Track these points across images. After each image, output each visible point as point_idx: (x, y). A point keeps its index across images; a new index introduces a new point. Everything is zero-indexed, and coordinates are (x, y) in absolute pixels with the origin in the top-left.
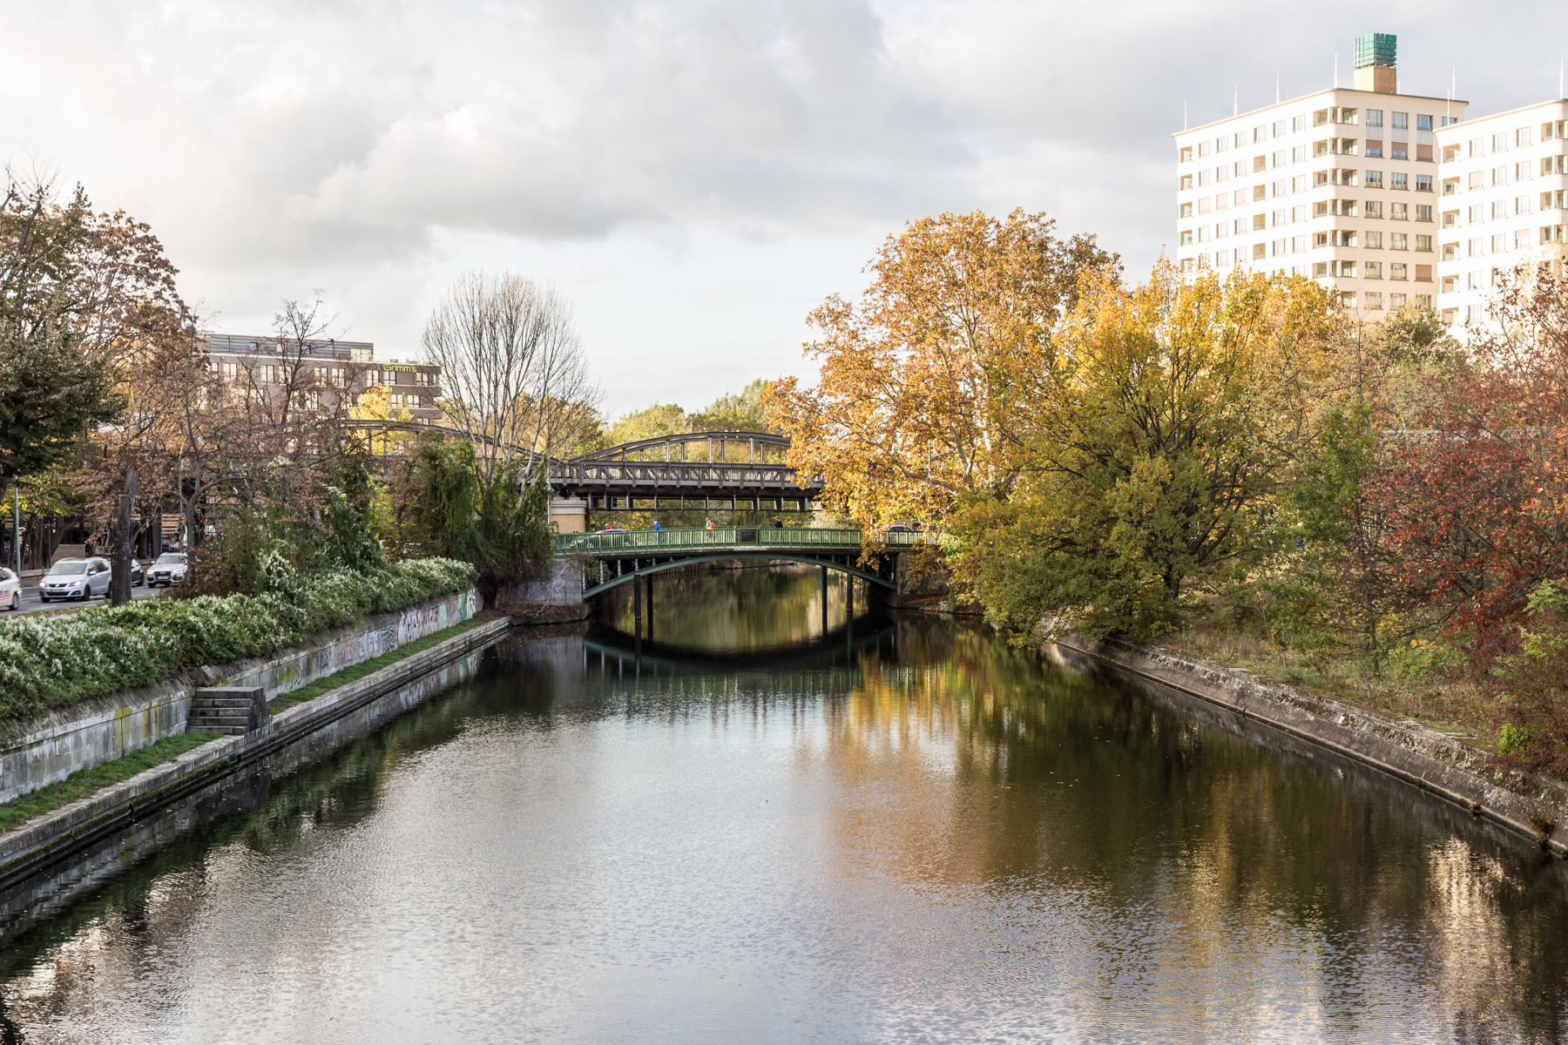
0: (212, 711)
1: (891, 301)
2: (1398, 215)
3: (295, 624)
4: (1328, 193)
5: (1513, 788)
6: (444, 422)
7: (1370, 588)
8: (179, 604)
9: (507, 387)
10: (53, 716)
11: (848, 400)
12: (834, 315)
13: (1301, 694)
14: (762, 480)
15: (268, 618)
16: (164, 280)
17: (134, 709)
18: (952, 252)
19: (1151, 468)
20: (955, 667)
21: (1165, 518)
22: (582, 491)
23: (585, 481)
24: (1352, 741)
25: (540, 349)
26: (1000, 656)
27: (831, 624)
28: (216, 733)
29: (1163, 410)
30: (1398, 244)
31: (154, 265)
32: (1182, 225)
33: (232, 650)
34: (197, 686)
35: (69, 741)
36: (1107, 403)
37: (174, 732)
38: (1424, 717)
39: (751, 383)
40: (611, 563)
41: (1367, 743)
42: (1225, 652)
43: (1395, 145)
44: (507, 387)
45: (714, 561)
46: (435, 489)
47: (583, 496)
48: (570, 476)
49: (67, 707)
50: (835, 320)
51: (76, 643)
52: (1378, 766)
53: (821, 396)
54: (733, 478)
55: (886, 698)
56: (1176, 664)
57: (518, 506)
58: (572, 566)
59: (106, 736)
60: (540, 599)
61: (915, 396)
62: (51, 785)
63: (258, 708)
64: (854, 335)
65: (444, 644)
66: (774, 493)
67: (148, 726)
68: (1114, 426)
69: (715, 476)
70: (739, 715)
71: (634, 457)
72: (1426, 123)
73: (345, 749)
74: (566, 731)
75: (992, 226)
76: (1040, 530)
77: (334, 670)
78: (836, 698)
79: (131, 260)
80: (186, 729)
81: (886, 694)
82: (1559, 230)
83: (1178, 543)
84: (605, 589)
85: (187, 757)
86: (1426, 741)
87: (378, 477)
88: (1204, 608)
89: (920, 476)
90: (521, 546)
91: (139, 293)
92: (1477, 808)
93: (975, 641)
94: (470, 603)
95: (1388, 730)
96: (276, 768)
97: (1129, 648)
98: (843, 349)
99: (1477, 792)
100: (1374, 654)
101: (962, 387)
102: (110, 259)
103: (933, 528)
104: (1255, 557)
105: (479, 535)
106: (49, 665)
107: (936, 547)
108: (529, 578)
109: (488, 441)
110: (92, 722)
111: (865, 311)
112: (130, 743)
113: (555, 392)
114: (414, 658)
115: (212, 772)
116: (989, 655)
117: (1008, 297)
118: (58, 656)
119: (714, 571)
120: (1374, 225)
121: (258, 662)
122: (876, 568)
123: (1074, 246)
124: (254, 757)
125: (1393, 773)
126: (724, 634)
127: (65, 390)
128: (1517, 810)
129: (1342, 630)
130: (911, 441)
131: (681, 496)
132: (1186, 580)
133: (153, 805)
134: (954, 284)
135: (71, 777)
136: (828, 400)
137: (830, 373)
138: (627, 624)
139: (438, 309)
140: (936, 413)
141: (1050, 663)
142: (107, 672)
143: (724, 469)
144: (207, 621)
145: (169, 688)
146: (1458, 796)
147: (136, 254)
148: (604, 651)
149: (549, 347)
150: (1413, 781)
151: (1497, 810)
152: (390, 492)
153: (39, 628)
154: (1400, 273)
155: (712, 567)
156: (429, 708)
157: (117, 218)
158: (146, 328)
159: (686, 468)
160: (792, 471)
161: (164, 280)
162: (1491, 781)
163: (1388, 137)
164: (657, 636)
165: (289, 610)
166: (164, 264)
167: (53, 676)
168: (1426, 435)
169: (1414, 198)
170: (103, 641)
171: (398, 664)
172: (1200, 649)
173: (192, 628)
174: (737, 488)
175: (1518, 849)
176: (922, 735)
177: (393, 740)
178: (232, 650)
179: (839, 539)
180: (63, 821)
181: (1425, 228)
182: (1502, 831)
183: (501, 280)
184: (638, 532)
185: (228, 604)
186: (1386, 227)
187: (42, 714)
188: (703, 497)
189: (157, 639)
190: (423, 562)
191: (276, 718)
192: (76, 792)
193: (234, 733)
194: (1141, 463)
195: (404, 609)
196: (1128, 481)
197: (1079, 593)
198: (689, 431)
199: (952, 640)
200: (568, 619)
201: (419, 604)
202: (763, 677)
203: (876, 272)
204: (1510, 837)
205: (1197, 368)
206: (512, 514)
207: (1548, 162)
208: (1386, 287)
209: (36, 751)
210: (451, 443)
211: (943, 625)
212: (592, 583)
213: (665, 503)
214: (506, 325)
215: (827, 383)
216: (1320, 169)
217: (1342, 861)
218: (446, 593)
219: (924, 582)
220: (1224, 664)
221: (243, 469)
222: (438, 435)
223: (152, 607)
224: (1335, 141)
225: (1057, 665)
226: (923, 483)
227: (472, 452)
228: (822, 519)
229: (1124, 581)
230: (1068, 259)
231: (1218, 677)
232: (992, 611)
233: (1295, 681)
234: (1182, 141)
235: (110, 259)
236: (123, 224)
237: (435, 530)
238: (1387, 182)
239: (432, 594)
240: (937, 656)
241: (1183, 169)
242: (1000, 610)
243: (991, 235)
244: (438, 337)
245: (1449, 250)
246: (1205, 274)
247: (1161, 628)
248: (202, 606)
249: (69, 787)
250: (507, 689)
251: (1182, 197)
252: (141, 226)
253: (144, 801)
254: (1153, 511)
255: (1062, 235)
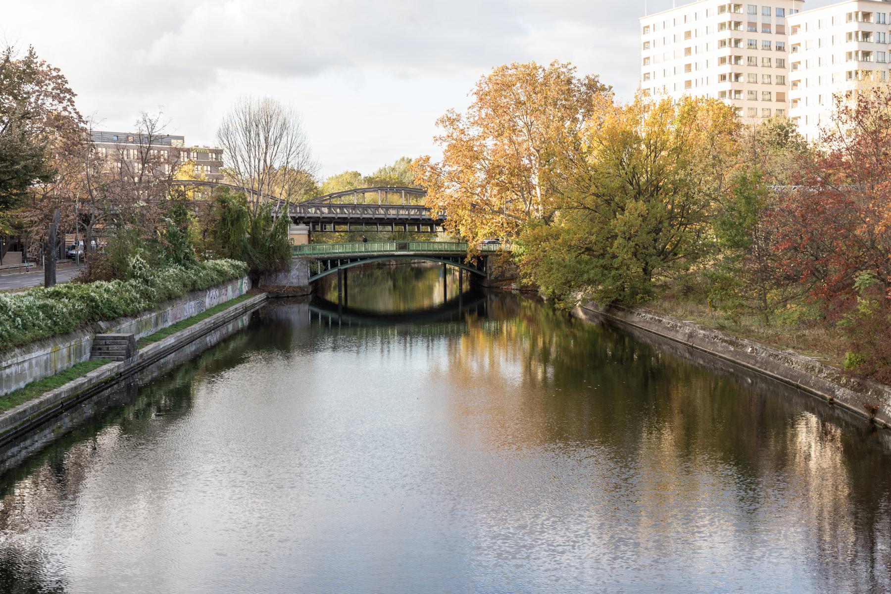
0: (105, 348)
1: (483, 112)
2: (766, 64)
3: (150, 297)
4: (726, 52)
5: (852, 388)
6: (226, 181)
7: (763, 275)
8: (84, 286)
9: (265, 161)
10: (17, 351)
11: (460, 169)
12: (451, 121)
13: (726, 335)
14: (409, 214)
15: (135, 294)
16: (69, 100)
17: (62, 346)
18: (518, 85)
19: (636, 207)
20: (521, 321)
21: (644, 236)
22: (306, 221)
23: (308, 215)
24: (757, 362)
25: (284, 140)
26: (548, 314)
27: (448, 297)
28: (107, 360)
29: (642, 175)
30: (766, 81)
31: (63, 92)
32: (645, 69)
33: (115, 312)
34: (96, 333)
35: (26, 365)
36: (611, 171)
37: (83, 360)
38: (798, 348)
39: (399, 159)
40: (324, 262)
41: (766, 363)
42: (680, 312)
43: (764, 25)
44: (265, 161)
45: (380, 260)
46: (224, 219)
47: (307, 223)
48: (300, 212)
49: (24, 346)
50: (452, 123)
51: (29, 308)
52: (772, 376)
53: (444, 166)
54: (392, 213)
55: (481, 339)
56: (651, 319)
57: (272, 229)
58: (302, 264)
59: (46, 362)
60: (284, 282)
61: (498, 166)
62: (16, 391)
63: (132, 345)
64: (462, 132)
65: (232, 308)
66: (416, 222)
67: (69, 356)
68: (617, 183)
69: (382, 212)
70: (396, 348)
71: (335, 201)
72: (781, 13)
73: (177, 368)
74: (299, 359)
75: (540, 70)
76: (573, 243)
77: (170, 324)
78: (453, 337)
79: (50, 89)
80: (90, 358)
81: (481, 336)
82: (857, 73)
83: (651, 250)
84: (315, 276)
85: (92, 374)
86: (799, 362)
87: (192, 213)
88: (665, 286)
89: (500, 211)
90: (274, 252)
91: (54, 107)
92: (832, 400)
93: (533, 306)
94: (244, 285)
95: (777, 356)
96: (142, 380)
97: (623, 310)
98: (456, 140)
99: (831, 391)
100: (765, 312)
101: (526, 161)
102: (37, 88)
103: (507, 242)
104: (694, 256)
105: (249, 246)
106: (14, 321)
107: (510, 252)
108: (277, 271)
109: (255, 193)
110: (39, 354)
111: (468, 118)
112: (59, 366)
113: (293, 164)
114: (215, 316)
115: (106, 383)
116: (542, 313)
117: (550, 110)
118: (19, 316)
119: (380, 266)
120: (752, 70)
121: (129, 319)
122: (475, 264)
123: (587, 82)
124: (130, 373)
125: (782, 380)
126: (386, 302)
127: (23, 163)
128: (854, 401)
129: (747, 299)
130: (495, 192)
131: (362, 223)
132: (655, 271)
133: (73, 402)
134: (519, 103)
135: (27, 386)
136: (447, 168)
137: (449, 154)
138: (333, 296)
139: (226, 117)
140: (512, 176)
141: (576, 318)
142: (46, 325)
143: (387, 208)
144: (101, 296)
145: (81, 334)
146: (820, 393)
147: (52, 85)
148: (320, 313)
149: (289, 138)
150: (793, 385)
151: (843, 401)
152: (199, 221)
153: (8, 300)
154: (767, 97)
155: (379, 264)
156: (223, 344)
157: (41, 65)
158: (59, 128)
159: (365, 207)
160: (429, 209)
161: (69, 100)
162: (839, 384)
163: (760, 20)
164: (349, 304)
165: (146, 289)
166: (69, 91)
167: (16, 327)
168: (793, 190)
169: (775, 55)
170: (43, 307)
171: (207, 320)
172: (665, 310)
173: (93, 300)
174: (395, 219)
175: (855, 423)
176: (503, 360)
177: (203, 363)
178: (115, 312)
179: (454, 248)
180: (25, 411)
181: (781, 72)
182: (847, 413)
183: (262, 100)
184: (336, 245)
185: (111, 285)
186: (759, 71)
187: (12, 350)
188: (376, 224)
189: (74, 306)
190: (218, 261)
191: (141, 351)
192: (31, 395)
193: (118, 360)
194: (630, 204)
195: (209, 288)
196: (622, 215)
197: (595, 278)
198: (366, 186)
199: (518, 305)
200: (300, 294)
201: (217, 286)
202: (412, 328)
203: (475, 96)
204: (852, 417)
205: (660, 151)
206: (268, 234)
207: (850, 35)
208: (760, 105)
209: (8, 371)
210: (232, 193)
211: (514, 297)
212: (314, 273)
213: (353, 227)
214: (262, 126)
215: (447, 159)
216: (722, 38)
217: (744, 433)
218: (232, 279)
219: (503, 273)
220: (680, 318)
221: (118, 209)
222: (226, 189)
223: (69, 287)
224: (730, 23)
225: (580, 319)
226: (501, 216)
227: (245, 198)
228: (442, 237)
229: (620, 272)
230: (583, 89)
231: (677, 326)
232: (543, 288)
233: (722, 328)
234: (644, 22)
235: (37, 88)
236: (45, 68)
237: (224, 243)
238: (759, 46)
239: (224, 280)
240: (510, 314)
241: (645, 38)
242: (547, 288)
243: (540, 75)
244: (226, 133)
245: (795, 84)
246: (665, 98)
247: (642, 298)
248: (97, 287)
249: (27, 392)
250: (267, 334)
251: (645, 54)
252: (55, 69)
253: (69, 399)
254: (637, 232)
255: (580, 75)
